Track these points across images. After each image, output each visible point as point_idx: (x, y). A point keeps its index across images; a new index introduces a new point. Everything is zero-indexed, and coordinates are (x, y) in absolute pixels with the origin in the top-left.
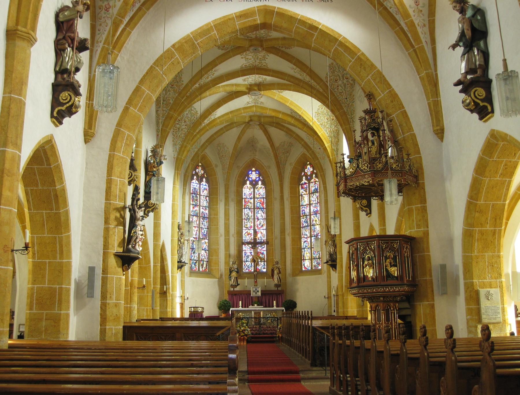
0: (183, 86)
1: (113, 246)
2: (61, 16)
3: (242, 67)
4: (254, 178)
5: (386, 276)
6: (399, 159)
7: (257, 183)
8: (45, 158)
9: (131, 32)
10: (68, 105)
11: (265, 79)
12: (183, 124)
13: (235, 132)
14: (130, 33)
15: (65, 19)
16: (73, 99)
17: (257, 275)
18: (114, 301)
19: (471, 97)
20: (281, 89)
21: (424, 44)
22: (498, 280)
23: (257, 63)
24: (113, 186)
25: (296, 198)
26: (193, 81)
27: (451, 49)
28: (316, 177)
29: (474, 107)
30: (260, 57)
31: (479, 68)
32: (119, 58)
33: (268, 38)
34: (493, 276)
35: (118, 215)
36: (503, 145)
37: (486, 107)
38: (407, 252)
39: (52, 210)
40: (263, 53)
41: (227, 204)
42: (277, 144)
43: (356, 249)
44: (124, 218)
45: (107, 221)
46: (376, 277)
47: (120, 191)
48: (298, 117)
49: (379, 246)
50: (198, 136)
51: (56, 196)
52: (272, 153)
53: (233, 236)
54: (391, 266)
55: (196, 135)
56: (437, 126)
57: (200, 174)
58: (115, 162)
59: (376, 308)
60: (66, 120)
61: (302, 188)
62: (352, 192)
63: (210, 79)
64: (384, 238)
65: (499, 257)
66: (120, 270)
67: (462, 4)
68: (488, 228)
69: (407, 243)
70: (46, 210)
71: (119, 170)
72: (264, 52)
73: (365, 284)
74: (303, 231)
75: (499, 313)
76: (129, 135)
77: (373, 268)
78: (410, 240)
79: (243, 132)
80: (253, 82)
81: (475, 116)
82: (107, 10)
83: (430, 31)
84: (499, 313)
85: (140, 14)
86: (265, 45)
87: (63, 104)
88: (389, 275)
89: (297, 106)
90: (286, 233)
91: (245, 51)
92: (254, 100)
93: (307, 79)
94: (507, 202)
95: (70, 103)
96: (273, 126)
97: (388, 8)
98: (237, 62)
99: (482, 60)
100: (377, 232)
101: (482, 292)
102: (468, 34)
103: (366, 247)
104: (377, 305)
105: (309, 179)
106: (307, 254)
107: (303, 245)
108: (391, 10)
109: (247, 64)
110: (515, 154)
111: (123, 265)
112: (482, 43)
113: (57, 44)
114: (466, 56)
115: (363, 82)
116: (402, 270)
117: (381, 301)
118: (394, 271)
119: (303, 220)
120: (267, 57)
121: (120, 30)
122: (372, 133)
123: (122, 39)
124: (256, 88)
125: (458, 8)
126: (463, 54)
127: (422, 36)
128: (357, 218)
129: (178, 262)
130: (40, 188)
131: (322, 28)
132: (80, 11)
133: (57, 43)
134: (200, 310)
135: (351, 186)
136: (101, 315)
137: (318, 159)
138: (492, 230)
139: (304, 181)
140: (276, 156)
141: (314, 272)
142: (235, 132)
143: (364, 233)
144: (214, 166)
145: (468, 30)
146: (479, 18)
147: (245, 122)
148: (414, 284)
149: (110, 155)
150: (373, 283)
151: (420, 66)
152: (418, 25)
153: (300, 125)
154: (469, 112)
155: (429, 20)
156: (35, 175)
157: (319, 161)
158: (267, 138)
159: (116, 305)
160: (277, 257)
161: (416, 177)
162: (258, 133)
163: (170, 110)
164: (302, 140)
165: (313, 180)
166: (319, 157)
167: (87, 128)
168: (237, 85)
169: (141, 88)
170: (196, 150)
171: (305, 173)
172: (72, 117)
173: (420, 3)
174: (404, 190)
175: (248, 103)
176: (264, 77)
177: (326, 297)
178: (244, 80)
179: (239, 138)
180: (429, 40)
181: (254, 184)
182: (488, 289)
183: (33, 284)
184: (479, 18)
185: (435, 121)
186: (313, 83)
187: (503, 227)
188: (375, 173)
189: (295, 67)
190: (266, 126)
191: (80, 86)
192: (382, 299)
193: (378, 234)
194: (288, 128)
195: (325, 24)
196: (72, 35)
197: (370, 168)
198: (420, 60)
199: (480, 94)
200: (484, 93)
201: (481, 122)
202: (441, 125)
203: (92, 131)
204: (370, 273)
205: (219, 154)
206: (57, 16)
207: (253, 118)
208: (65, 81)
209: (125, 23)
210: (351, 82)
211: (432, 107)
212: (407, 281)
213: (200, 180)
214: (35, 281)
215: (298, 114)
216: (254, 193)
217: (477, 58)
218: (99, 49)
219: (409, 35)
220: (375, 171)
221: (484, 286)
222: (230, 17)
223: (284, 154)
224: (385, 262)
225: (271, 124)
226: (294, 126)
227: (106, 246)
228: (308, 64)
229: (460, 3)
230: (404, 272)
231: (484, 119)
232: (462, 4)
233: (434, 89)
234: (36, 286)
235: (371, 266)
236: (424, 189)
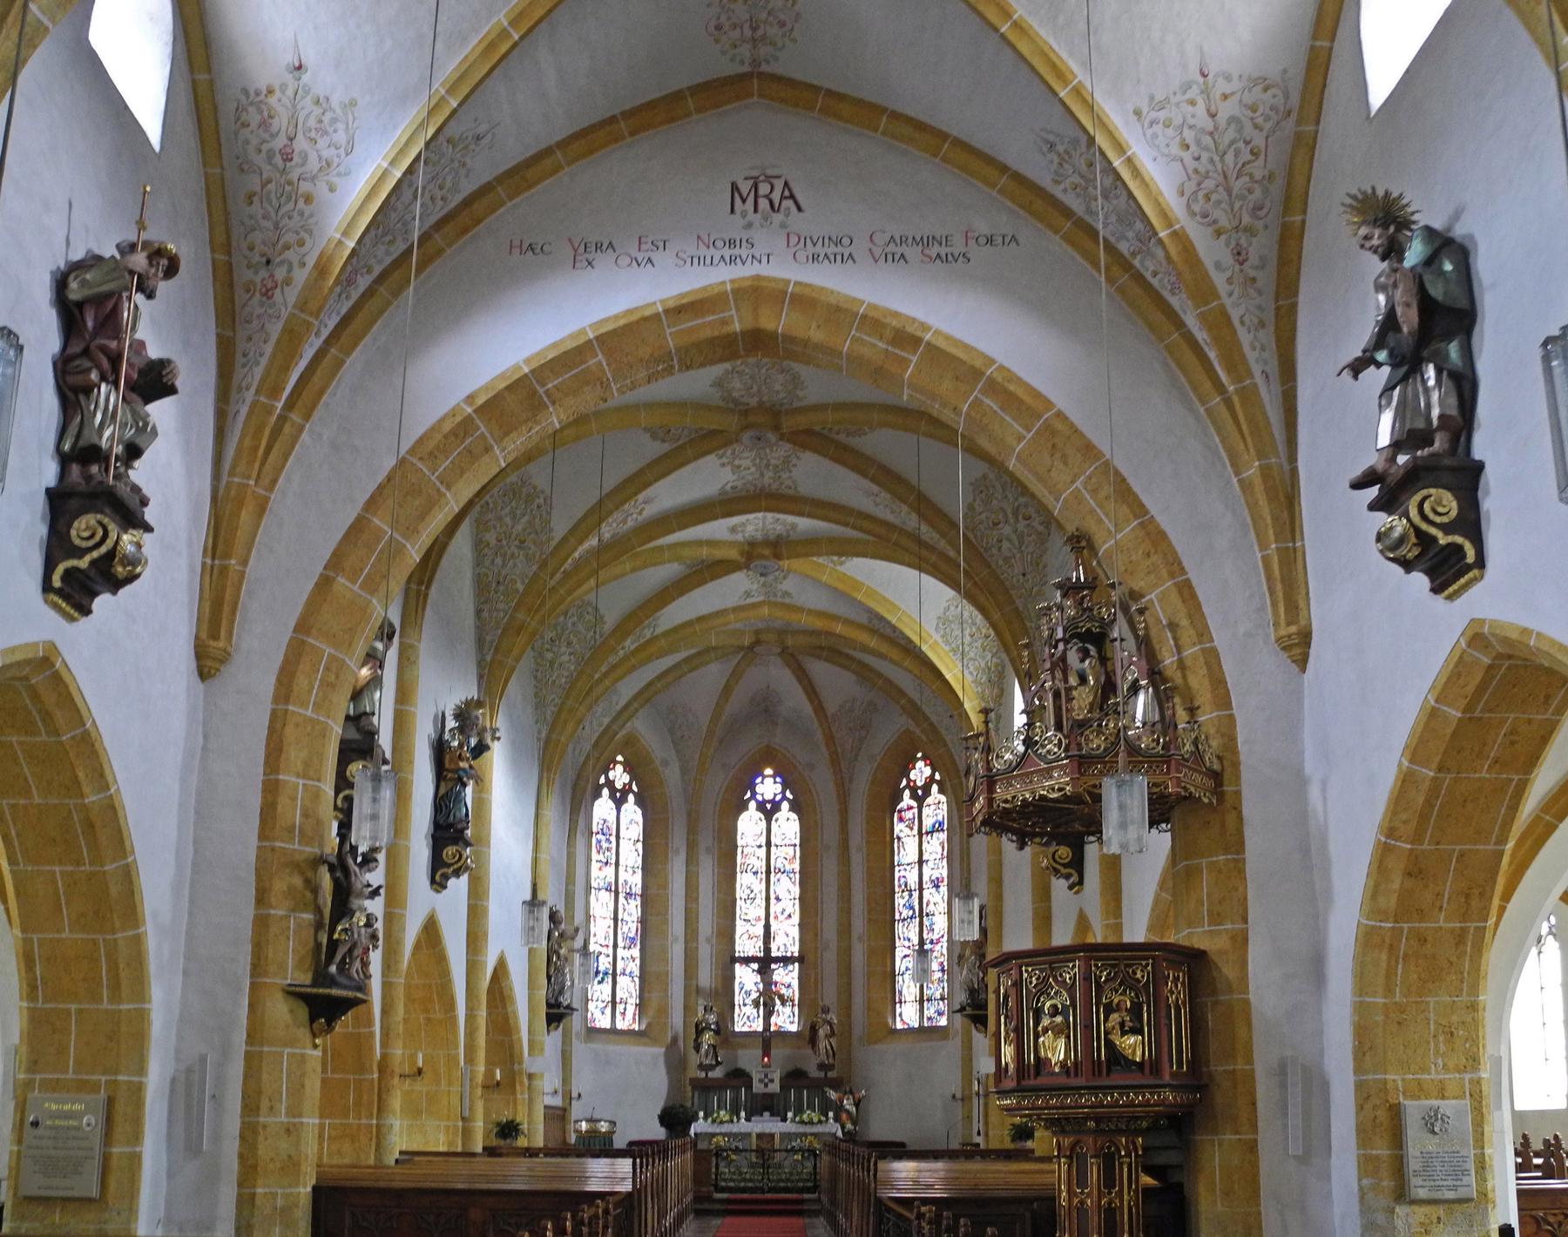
0: (554, 543)
1: (282, 967)
2: (73, 285)
3: (723, 492)
4: (769, 796)
5: (1108, 1059)
6: (1164, 724)
7: (776, 806)
8: (39, 712)
9: (343, 362)
10: (95, 554)
11: (794, 526)
12: (563, 649)
13: (714, 674)
14: (340, 364)
15: (87, 292)
16: (113, 536)
17: (768, 1039)
18: (284, 1119)
19: (1409, 520)
20: (840, 555)
21: (1259, 380)
22: (1467, 1076)
23: (767, 480)
24: (283, 801)
25: (885, 845)
26: (580, 530)
27: (1347, 375)
28: (941, 791)
29: (1416, 551)
30: (773, 462)
31: (1440, 428)
32: (305, 436)
33: (795, 405)
34: (1451, 1065)
35: (298, 881)
36: (1509, 668)
37: (1458, 550)
38: (1175, 991)
39: (78, 863)
40: (784, 449)
41: (691, 860)
42: (831, 708)
43: (1015, 984)
44: (315, 890)
45: (261, 898)
46: (1076, 1063)
47: (305, 815)
48: (888, 631)
49: (1087, 978)
50: (607, 682)
51: (90, 826)
52: (819, 731)
53: (708, 940)
54: (1124, 1033)
55: (600, 681)
56: (1289, 624)
57: (619, 785)
58: (290, 732)
59: (1072, 1148)
60: (103, 603)
61: (901, 820)
62: (1014, 820)
63: (630, 523)
64: (1118, 955)
65: (1473, 1007)
66: (303, 1033)
67: (1392, 229)
68: (1442, 923)
69: (1176, 965)
70: (60, 862)
71: (304, 754)
72: (788, 446)
73: (1041, 1081)
74: (900, 929)
75: (1465, 1172)
76: (332, 658)
77: (1068, 1037)
78: (1194, 961)
79: (736, 675)
80: (759, 535)
81: (1420, 580)
82: (268, 294)
83: (1278, 340)
84: (1465, 1172)
85: (372, 305)
86: (788, 423)
87: (80, 553)
88: (1116, 1058)
89: (886, 600)
90: (855, 935)
91: (727, 444)
92: (764, 585)
93: (911, 521)
94: (1510, 845)
95: (103, 549)
96: (819, 657)
97: (1148, 276)
98: (707, 477)
99: (1453, 401)
100: (1098, 936)
101: (1413, 1110)
102: (1409, 319)
103: (1046, 979)
104: (1077, 1143)
105: (921, 795)
106: (908, 988)
107: (900, 965)
108: (1155, 282)
109: (739, 484)
110: (1547, 698)
111: (312, 1020)
112: (1454, 350)
113: (64, 372)
114: (1397, 392)
115: (1057, 500)
116: (1158, 1042)
117: (1090, 1132)
118: (1132, 1045)
119: (902, 902)
120: (794, 461)
121: (308, 354)
122: (1079, 650)
123: (317, 379)
124: (766, 552)
125: (1375, 242)
126: (1388, 389)
127: (1251, 356)
128: (1043, 895)
129: (549, 1005)
130: (37, 800)
131: (934, 341)
132: (138, 269)
133: (64, 367)
134: (604, 1127)
135: (1006, 801)
136: (241, 1156)
137: (946, 745)
138: (1453, 930)
139: (907, 800)
140: (830, 739)
141: (925, 1032)
142: (714, 674)
143: (1062, 936)
144: (658, 762)
145: (1408, 305)
146: (1448, 267)
147: (741, 648)
148: (1197, 1080)
149: (274, 714)
150: (1064, 1081)
151: (1242, 447)
152: (1242, 323)
153: (895, 654)
154: (1399, 570)
155: (1278, 309)
156: (16, 761)
157: (948, 750)
158: (805, 689)
159: (288, 1130)
160: (830, 996)
161: (1217, 776)
162: (780, 678)
163: (515, 609)
164: (903, 694)
165: (929, 800)
166: (948, 739)
167: (204, 635)
168: (710, 543)
169: (370, 521)
170: (606, 721)
171: (909, 780)
172: (122, 592)
173: (1251, 256)
174: (1176, 814)
175: (748, 594)
176: (791, 519)
177: (959, 1095)
178: (733, 530)
179: (727, 691)
180: (1273, 367)
181: (769, 810)
182: (1435, 1103)
183: (30, 1070)
184: (1448, 267)
185: (1282, 610)
186: (926, 532)
187: (1491, 921)
188: (1082, 762)
189: (875, 488)
190: (800, 658)
191: (144, 502)
192: (1091, 1124)
193: (1100, 940)
194: (860, 662)
195: (945, 327)
196: (113, 344)
197: (1066, 750)
198: (1244, 427)
199: (1440, 510)
200: (1454, 504)
201: (1439, 600)
202: (1303, 622)
203: (221, 644)
204: (1056, 1051)
205: (671, 731)
206: (61, 283)
207: (763, 637)
208: (93, 483)
209: (325, 333)
210: (1041, 528)
211: (1276, 567)
212: (1173, 1075)
213: (619, 800)
214: (35, 1062)
215: (889, 623)
216: (769, 838)
217: (1435, 396)
218: (244, 410)
219: (1212, 355)
220: (1081, 757)
221: (1419, 1091)
222: (647, 313)
223: (850, 733)
224: (1106, 1020)
225: (818, 652)
226: (873, 652)
227: (258, 967)
228: (914, 482)
229: (1385, 226)
230: (1165, 1049)
231: (1451, 589)
232: (1392, 229)
233: (1285, 515)
234: (38, 1077)
235: (1059, 1031)
236: (1237, 809)
